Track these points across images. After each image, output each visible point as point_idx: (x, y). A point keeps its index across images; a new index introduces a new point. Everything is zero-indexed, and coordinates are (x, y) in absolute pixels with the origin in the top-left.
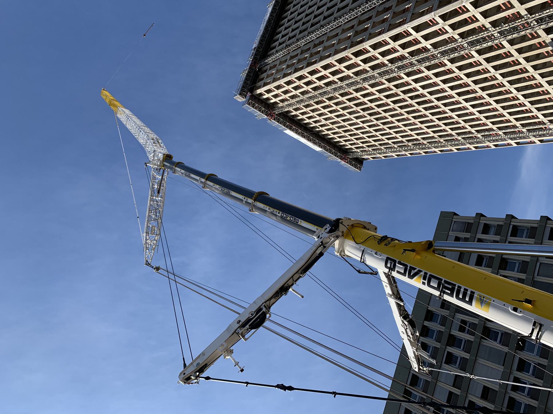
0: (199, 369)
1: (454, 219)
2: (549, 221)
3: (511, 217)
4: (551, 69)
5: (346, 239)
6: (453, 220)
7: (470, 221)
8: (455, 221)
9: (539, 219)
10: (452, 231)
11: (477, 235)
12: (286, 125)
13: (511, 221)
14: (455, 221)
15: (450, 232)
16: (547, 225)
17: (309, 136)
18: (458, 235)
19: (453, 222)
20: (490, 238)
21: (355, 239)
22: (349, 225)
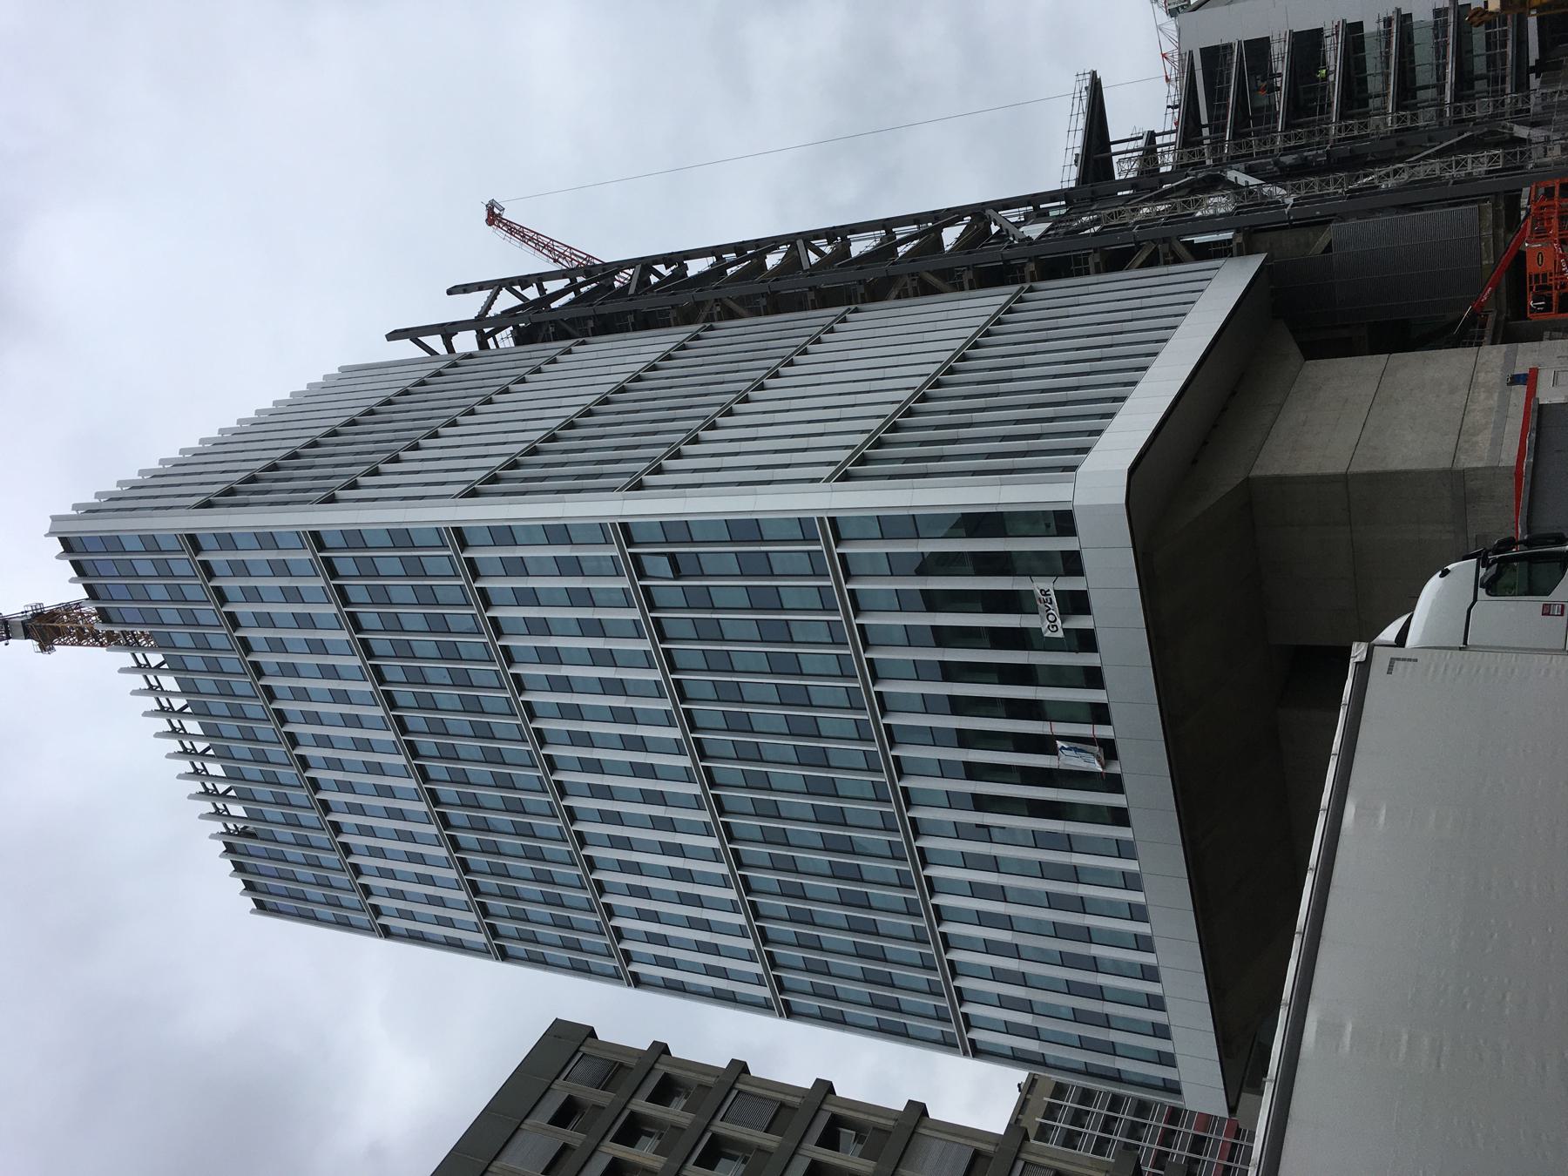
1: (662, 1064)
2: (664, 1056)
3: (661, 1049)
6: (582, 1049)
8: (584, 1054)
10: (564, 1080)
11: (634, 1101)
13: (824, 1098)
14: (584, 1054)
16: (825, 1107)
18: (574, 1093)
19: (580, 1055)
20: (666, 1116)
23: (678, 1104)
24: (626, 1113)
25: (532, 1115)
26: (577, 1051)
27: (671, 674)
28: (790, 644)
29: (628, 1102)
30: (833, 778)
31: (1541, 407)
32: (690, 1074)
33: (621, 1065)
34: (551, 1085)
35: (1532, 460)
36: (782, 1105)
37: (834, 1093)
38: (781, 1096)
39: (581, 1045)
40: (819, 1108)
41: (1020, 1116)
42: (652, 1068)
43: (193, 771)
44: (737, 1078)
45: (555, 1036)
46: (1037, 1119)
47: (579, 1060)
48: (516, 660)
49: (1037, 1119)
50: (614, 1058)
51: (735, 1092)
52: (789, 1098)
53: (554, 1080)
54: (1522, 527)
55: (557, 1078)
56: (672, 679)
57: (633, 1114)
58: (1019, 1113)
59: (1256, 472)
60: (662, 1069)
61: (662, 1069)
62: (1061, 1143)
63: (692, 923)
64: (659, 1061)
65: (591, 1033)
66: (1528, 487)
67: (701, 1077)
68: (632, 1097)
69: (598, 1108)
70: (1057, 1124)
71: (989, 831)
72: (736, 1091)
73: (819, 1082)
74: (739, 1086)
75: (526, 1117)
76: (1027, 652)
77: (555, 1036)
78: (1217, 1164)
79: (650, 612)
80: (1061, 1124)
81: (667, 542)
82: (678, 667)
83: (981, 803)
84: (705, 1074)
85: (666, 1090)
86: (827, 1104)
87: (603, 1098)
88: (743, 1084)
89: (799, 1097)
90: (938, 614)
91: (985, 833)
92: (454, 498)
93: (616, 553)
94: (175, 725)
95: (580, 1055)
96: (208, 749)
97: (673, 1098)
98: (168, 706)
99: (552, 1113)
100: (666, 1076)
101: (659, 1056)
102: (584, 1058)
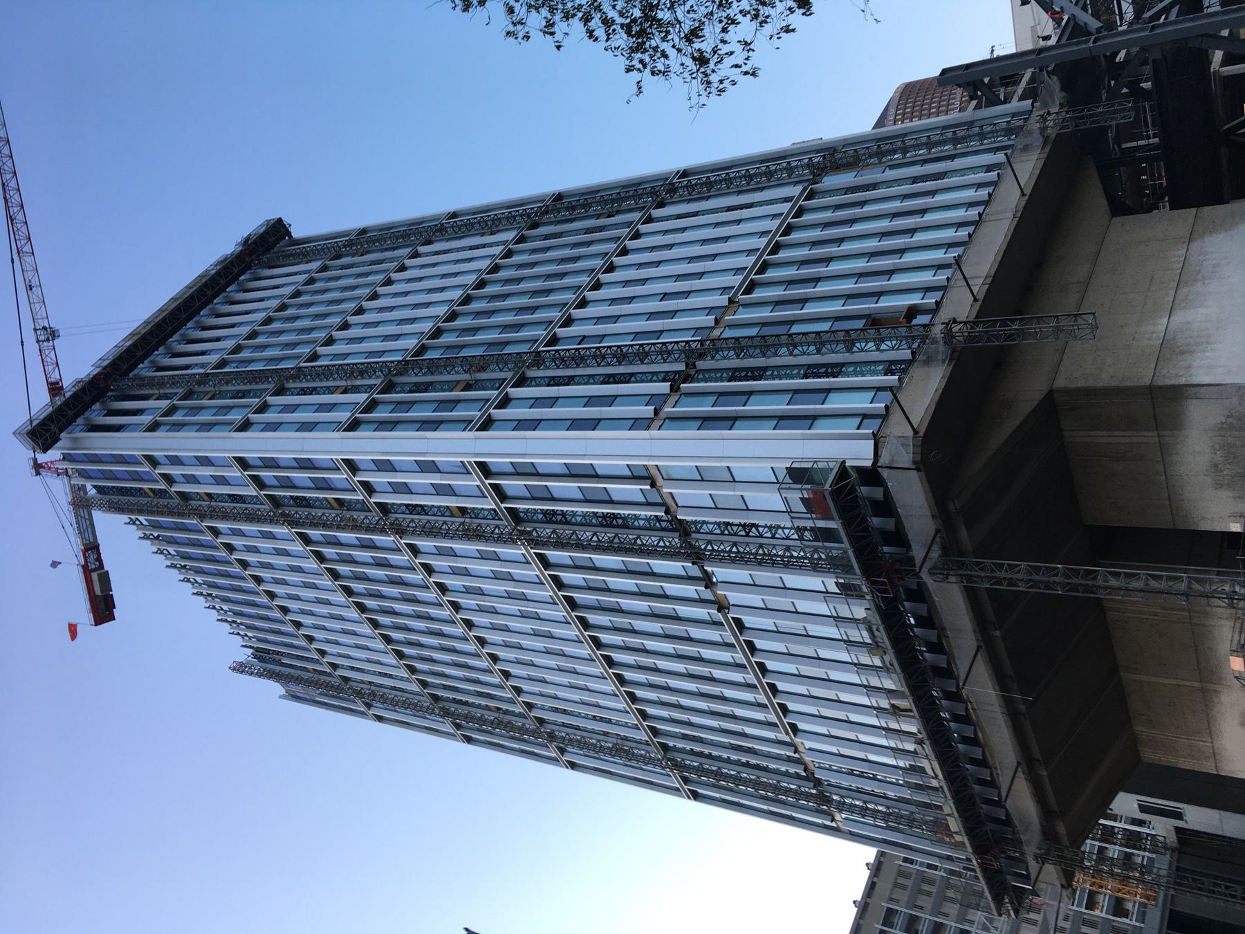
5: (1208, 240)
59: (1061, 383)
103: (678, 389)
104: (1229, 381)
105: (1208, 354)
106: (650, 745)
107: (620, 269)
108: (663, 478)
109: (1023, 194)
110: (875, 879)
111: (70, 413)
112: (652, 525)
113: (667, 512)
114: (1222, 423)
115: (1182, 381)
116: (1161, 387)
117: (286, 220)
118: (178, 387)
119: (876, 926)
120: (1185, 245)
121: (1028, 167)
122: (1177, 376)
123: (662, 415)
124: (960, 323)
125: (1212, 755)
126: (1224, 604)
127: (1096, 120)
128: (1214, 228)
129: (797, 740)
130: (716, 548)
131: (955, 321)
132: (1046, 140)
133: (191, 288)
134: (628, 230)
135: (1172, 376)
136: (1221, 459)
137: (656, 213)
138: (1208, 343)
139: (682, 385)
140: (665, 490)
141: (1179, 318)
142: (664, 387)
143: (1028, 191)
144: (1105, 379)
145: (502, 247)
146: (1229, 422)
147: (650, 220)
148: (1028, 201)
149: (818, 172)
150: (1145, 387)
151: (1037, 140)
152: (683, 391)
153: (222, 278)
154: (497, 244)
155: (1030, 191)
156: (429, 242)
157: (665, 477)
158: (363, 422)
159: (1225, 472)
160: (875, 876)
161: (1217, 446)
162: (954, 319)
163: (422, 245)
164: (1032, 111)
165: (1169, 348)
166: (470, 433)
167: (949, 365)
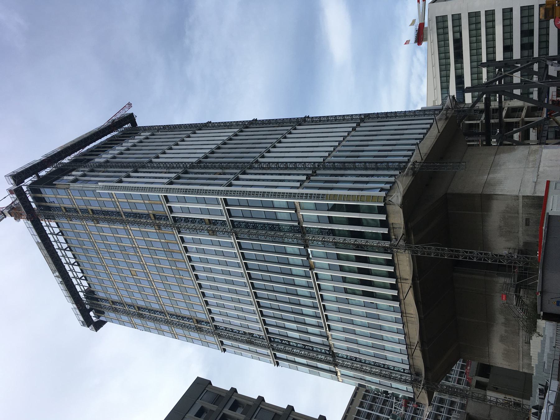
0: (324, 228)
2: (235, 393)
3: (234, 390)
4: (512, 120)
5: (501, 155)
6: (207, 388)
7: (278, 412)
8: (207, 391)
9: (256, 398)
10: (200, 400)
11: (225, 409)
12: (42, 234)
14: (207, 391)
15: (197, 400)
16: (291, 416)
17: (58, 260)
18: (204, 405)
19: (206, 391)
20: (236, 416)
21: (275, 216)
22: (549, 304)
23: (240, 410)
24: (222, 414)
25: (188, 413)
26: (205, 389)
27: (229, 218)
28: (273, 208)
29: (222, 410)
30: (288, 258)
31: (550, 217)
32: (244, 400)
33: (220, 395)
34: (195, 402)
35: (545, 241)
36: (276, 414)
37: (294, 411)
38: (275, 411)
39: (206, 387)
40: (289, 416)
41: (357, 391)
42: (231, 397)
43: (62, 255)
44: (260, 403)
45: (198, 383)
46: (363, 392)
47: (206, 392)
48: (174, 211)
49: (363, 392)
50: (218, 393)
51: (260, 408)
52: (278, 411)
53: (197, 400)
54: (540, 271)
55: (198, 399)
56: (230, 220)
57: (224, 414)
58: (357, 390)
59: (449, 191)
60: (234, 398)
61: (234, 398)
62: (371, 401)
63: (230, 291)
64: (208, 387)
65: (210, 383)
66: (543, 254)
67: (248, 402)
68: (223, 408)
69: (212, 411)
70: (370, 394)
71: (348, 300)
72: (260, 408)
73: (289, 406)
74: (261, 406)
75: (187, 413)
76: (361, 227)
77: (198, 383)
78: (433, 412)
79: (229, 218)
80: (371, 395)
81: (243, 217)
82: (242, 247)
83: (346, 291)
84: (249, 401)
85: (236, 406)
86: (292, 414)
87: (214, 408)
88: (262, 405)
89: (282, 411)
90: (332, 224)
91: (347, 302)
92: (164, 184)
93: (222, 208)
94: (78, 282)
95: (206, 391)
96: (75, 263)
97: (238, 408)
98: (53, 232)
99: (195, 413)
100: (236, 400)
101: (233, 393)
102: (207, 392)
103: (310, 179)
104: (508, 194)
105: (501, 186)
106: (265, 339)
107: (266, 158)
108: (300, 209)
109: (439, 132)
110: (347, 414)
111: (57, 159)
112: (292, 229)
113: (299, 224)
114: (505, 210)
115: (492, 193)
116: (485, 194)
117: (135, 114)
118: (84, 167)
119: (353, 416)
120: (494, 156)
121: (441, 125)
122: (490, 191)
123: (303, 186)
124: (418, 162)
125: (488, 355)
126: (475, 394)
127: (436, 168)
128: (504, 152)
129: (329, 333)
130: (243, 338)
131: (416, 162)
132: (446, 119)
133: (72, 142)
134: (260, 154)
135: (488, 191)
136: (503, 224)
137: (298, 127)
138: (501, 183)
139: (311, 177)
140: (301, 213)
141: (491, 176)
142: (304, 178)
143: (441, 131)
144: (466, 191)
145: (169, 180)
146: (507, 210)
147: (238, 179)
148: (440, 134)
149: (362, 120)
150: (479, 194)
151: (411, 172)
152: (311, 179)
153: (63, 153)
154: (165, 178)
155: (442, 131)
156: (200, 130)
157: (301, 209)
158: (174, 183)
159: (504, 230)
160: (347, 413)
161: (502, 219)
162: (416, 161)
163: (198, 130)
164: (433, 123)
165: (487, 184)
166: (223, 187)
167: (413, 177)
